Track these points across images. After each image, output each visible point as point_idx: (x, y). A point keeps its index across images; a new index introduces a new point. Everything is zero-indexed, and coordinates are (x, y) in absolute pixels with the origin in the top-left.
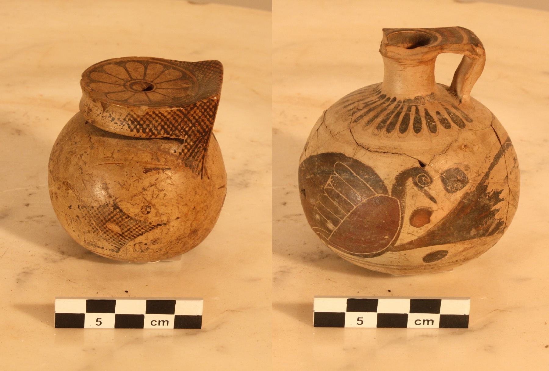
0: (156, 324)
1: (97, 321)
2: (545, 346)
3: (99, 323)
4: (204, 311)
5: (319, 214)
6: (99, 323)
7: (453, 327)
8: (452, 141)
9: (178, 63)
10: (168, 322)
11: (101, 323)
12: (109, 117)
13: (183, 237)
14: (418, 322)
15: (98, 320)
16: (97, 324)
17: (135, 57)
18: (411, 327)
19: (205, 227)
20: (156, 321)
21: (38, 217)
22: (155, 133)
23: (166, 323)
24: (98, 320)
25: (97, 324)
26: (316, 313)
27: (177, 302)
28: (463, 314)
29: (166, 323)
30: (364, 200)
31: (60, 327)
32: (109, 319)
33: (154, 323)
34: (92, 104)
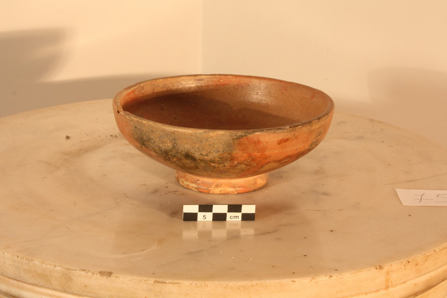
0: (232, 218)
1: (204, 217)
2: (379, 265)
5: (264, 129)
8: (243, 85)
10: (238, 217)
11: (206, 218)
12: (202, 143)
14: (231, 218)
15: (204, 216)
16: (204, 219)
18: (228, 220)
20: (232, 217)
21: (174, 192)
23: (237, 217)
24: (204, 216)
25: (204, 219)
26: (184, 213)
28: (252, 213)
29: (237, 217)
31: (246, 220)
32: (209, 216)
33: (231, 218)
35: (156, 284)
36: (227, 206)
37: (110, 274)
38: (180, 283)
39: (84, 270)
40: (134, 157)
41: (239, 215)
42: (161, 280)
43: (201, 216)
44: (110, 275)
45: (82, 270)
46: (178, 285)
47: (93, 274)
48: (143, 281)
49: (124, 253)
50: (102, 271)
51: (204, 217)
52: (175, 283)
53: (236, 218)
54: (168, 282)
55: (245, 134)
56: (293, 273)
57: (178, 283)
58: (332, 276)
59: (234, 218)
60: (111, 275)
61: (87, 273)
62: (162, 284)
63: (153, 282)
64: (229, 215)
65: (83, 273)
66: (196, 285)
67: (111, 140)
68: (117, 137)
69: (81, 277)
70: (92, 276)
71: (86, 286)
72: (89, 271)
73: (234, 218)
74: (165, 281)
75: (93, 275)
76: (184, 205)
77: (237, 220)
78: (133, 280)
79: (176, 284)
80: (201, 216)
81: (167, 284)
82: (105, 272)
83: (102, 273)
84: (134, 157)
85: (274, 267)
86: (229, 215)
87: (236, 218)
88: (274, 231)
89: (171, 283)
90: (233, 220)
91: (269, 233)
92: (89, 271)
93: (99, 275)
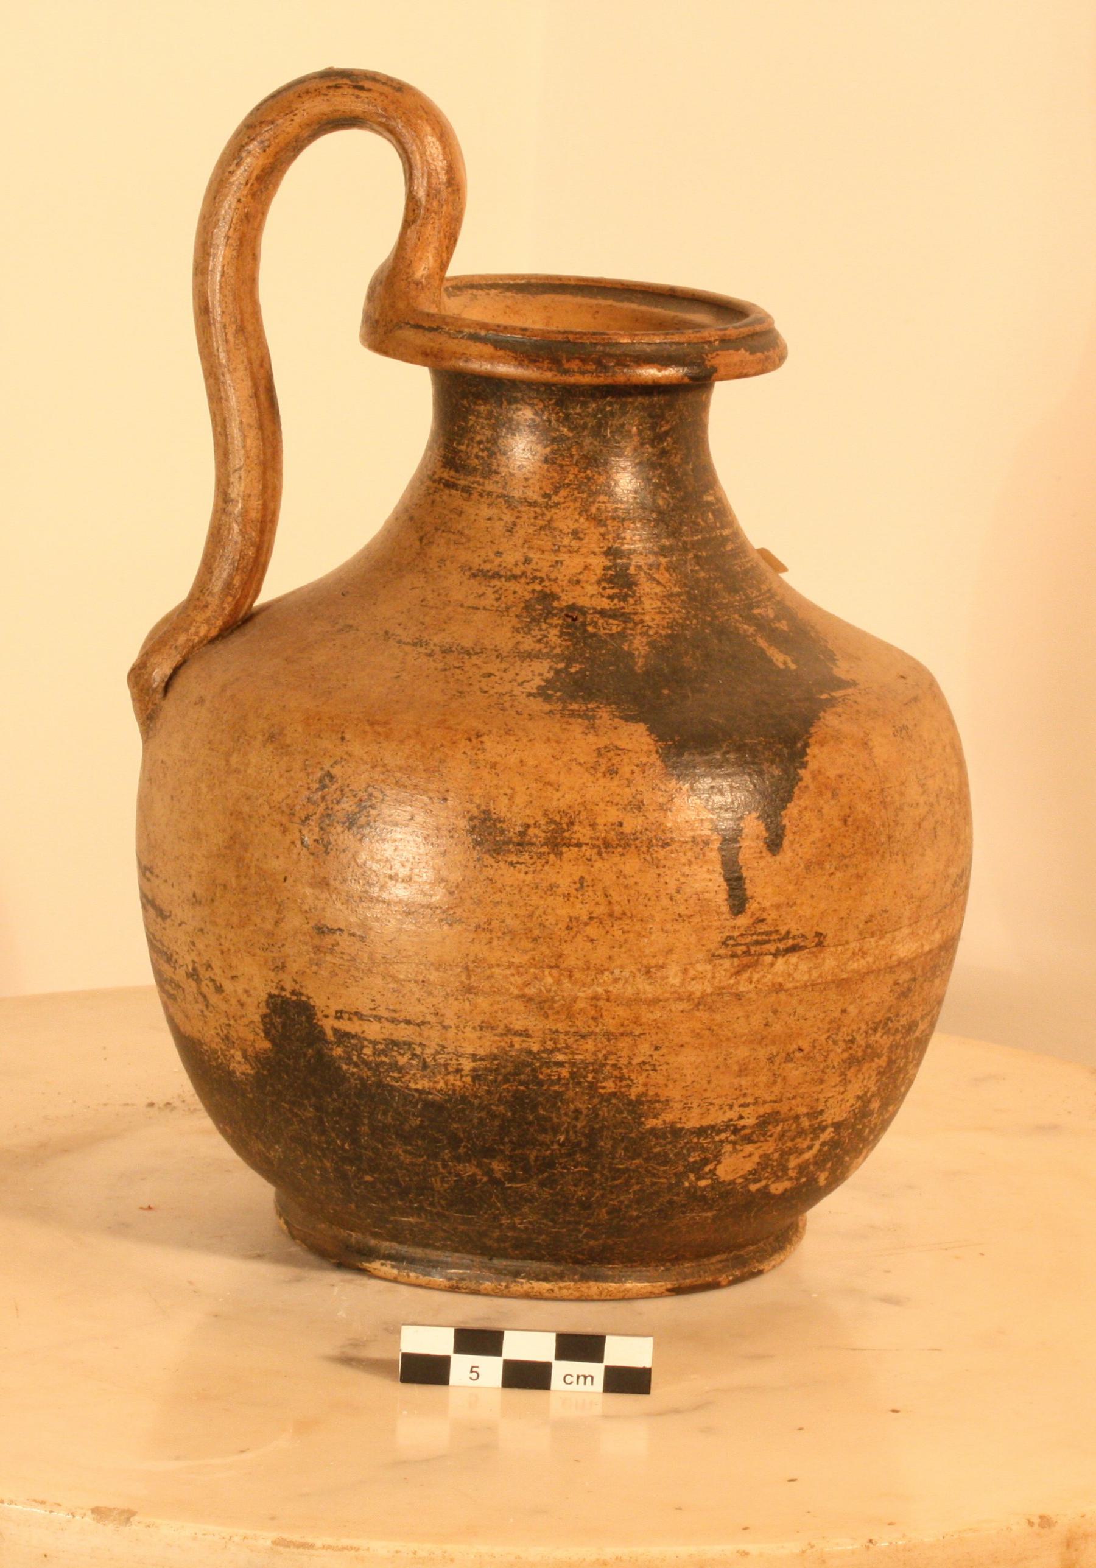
0: (571, 1383)
1: (472, 1371)
3: (474, 1375)
4: (656, 1356)
6: (474, 1375)
7: (822, 1178)
9: (723, 1279)
10: (592, 1377)
11: (478, 1376)
13: (898, 998)
15: (474, 1369)
16: (471, 1379)
17: (559, 278)
19: (669, 1117)
22: (492, 364)
23: (589, 1379)
24: (474, 1369)
25: (471, 1379)
27: (507, 1335)
29: (589, 1379)
30: (443, 1171)
32: (491, 1368)
33: (569, 1380)
34: (431, 566)
35: (281, 1548)
36: (553, 1336)
37: (127, 1516)
38: (359, 1549)
39: (43, 1503)
40: (228, 1171)
41: (597, 1370)
42: (296, 1537)
43: (461, 1365)
44: (128, 1519)
45: (35, 1501)
46: (353, 1553)
47: (72, 1514)
48: (236, 1539)
49: (178, 1458)
50: (101, 1504)
51: (472, 1371)
52: (343, 1548)
53: (585, 1383)
54: (319, 1543)
55: (564, 1079)
56: (747, 1531)
57: (352, 1548)
58: (876, 1543)
59: (578, 1383)
60: (131, 1519)
61: (51, 1512)
62: (301, 1550)
63: (269, 1543)
64: (561, 1369)
65: (39, 1511)
66: (412, 1555)
67: (150, 1118)
68: (175, 1108)
69: (30, 1526)
70: (69, 1521)
71: (46, 1556)
72: (59, 1505)
73: (578, 1383)
74: (309, 1540)
75: (70, 1516)
76: (404, 1324)
77: (588, 1387)
78: (205, 1534)
79: (346, 1551)
80: (461, 1365)
81: (317, 1549)
82: (111, 1510)
83: (99, 1513)
84: (228, 1171)
85: (680, 1509)
86: (561, 1369)
87: (585, 1383)
88: (698, 1407)
89: (330, 1547)
90: (574, 1386)
91: (677, 1411)
92: (59, 1505)
93: (89, 1519)
